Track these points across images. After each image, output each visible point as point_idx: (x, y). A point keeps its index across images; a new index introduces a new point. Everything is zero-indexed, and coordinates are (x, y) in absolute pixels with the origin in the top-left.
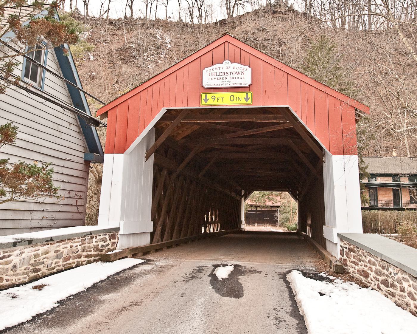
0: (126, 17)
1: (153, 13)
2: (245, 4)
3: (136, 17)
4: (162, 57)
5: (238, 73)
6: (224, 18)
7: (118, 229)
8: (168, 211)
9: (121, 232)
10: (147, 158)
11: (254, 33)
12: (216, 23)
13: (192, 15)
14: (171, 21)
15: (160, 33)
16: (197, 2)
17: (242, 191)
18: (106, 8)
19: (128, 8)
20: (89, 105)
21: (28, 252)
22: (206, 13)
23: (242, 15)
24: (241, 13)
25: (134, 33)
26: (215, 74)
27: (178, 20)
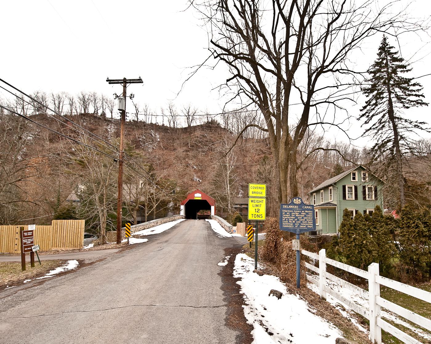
3: (139, 120)
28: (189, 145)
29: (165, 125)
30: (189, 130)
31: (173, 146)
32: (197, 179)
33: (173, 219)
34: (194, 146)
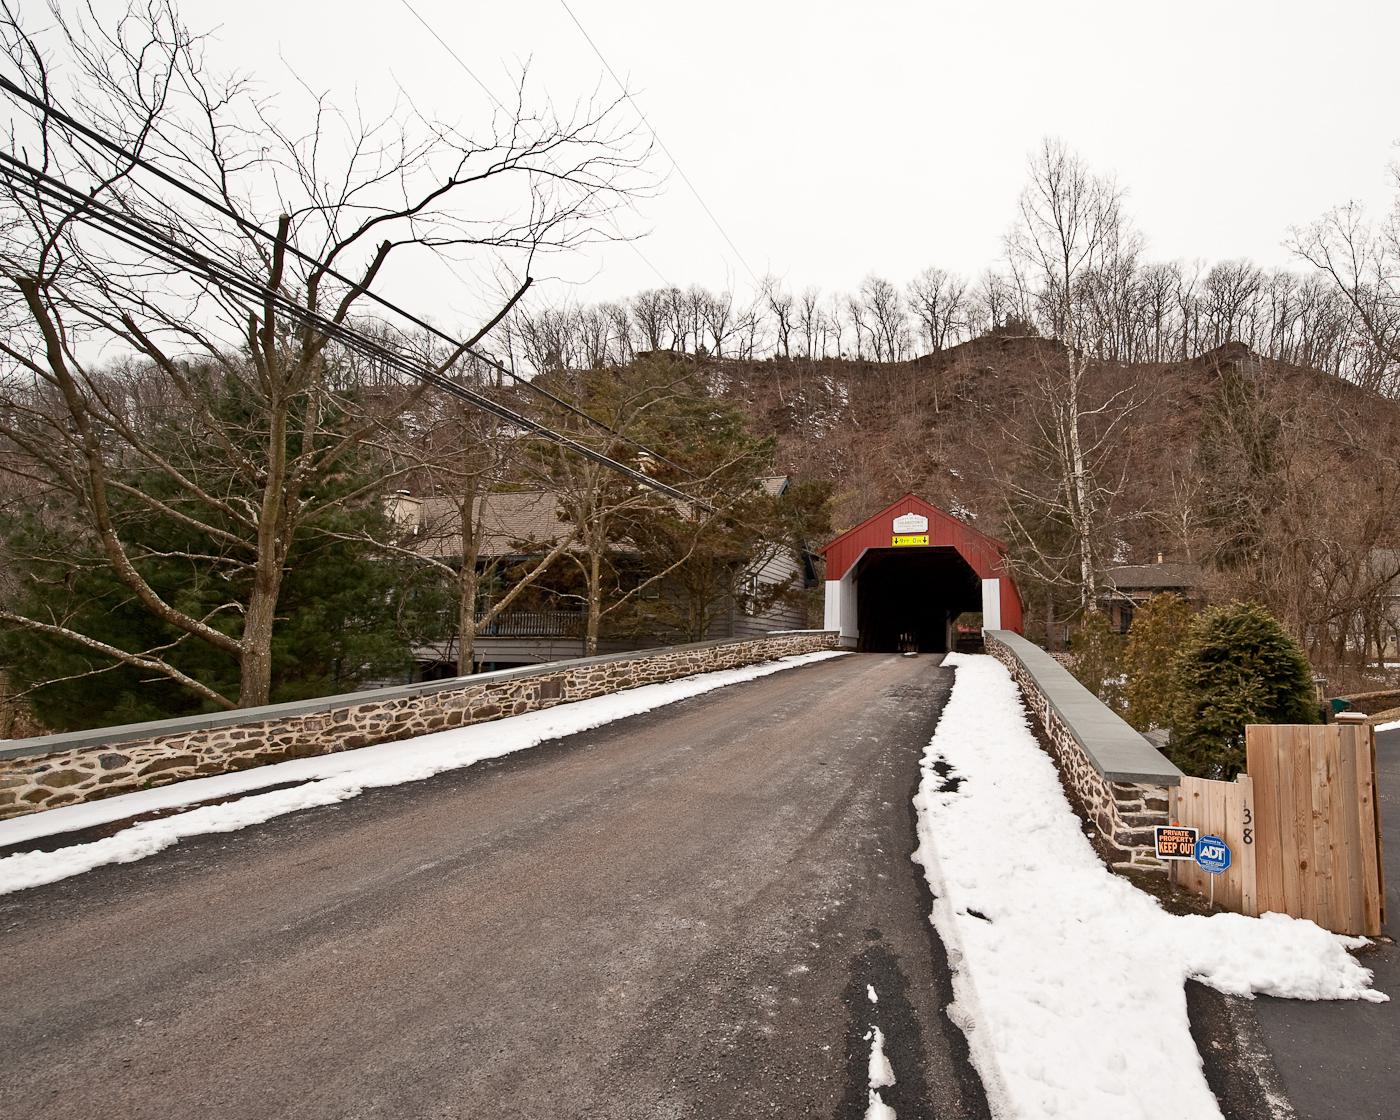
2: (960, 328)
9: (841, 634)
10: (853, 582)
17: (150, 358)
19: (782, 344)
20: (431, 333)
21: (799, 639)
24: (955, 343)
29: (866, 359)
30: (937, 361)
31: (886, 416)
32: (962, 510)
34: (950, 405)
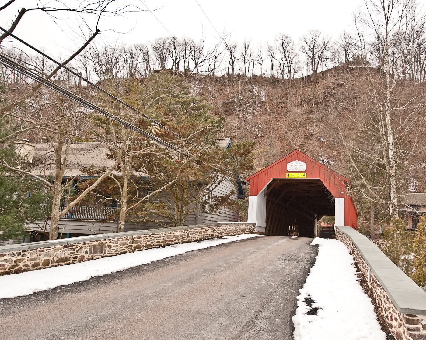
0: (228, 74)
1: (251, 71)
3: (236, 73)
4: (258, 108)
5: (301, 166)
6: (309, 74)
7: (255, 224)
8: (272, 221)
9: (256, 225)
10: (264, 197)
11: (334, 88)
12: (303, 79)
13: (282, 72)
14: (265, 77)
15: (256, 88)
16: (287, 61)
18: (212, 67)
22: (294, 69)
23: (324, 72)
24: (324, 69)
25: (235, 89)
26: (292, 166)
27: (271, 76)
28: (313, 102)
33: (209, 232)
